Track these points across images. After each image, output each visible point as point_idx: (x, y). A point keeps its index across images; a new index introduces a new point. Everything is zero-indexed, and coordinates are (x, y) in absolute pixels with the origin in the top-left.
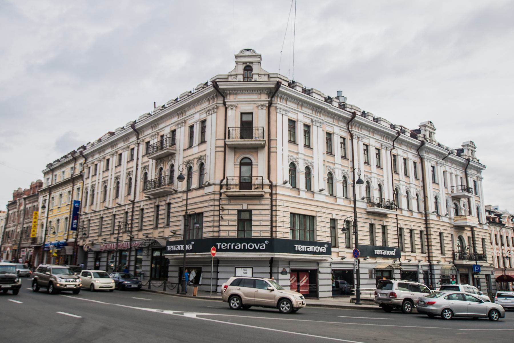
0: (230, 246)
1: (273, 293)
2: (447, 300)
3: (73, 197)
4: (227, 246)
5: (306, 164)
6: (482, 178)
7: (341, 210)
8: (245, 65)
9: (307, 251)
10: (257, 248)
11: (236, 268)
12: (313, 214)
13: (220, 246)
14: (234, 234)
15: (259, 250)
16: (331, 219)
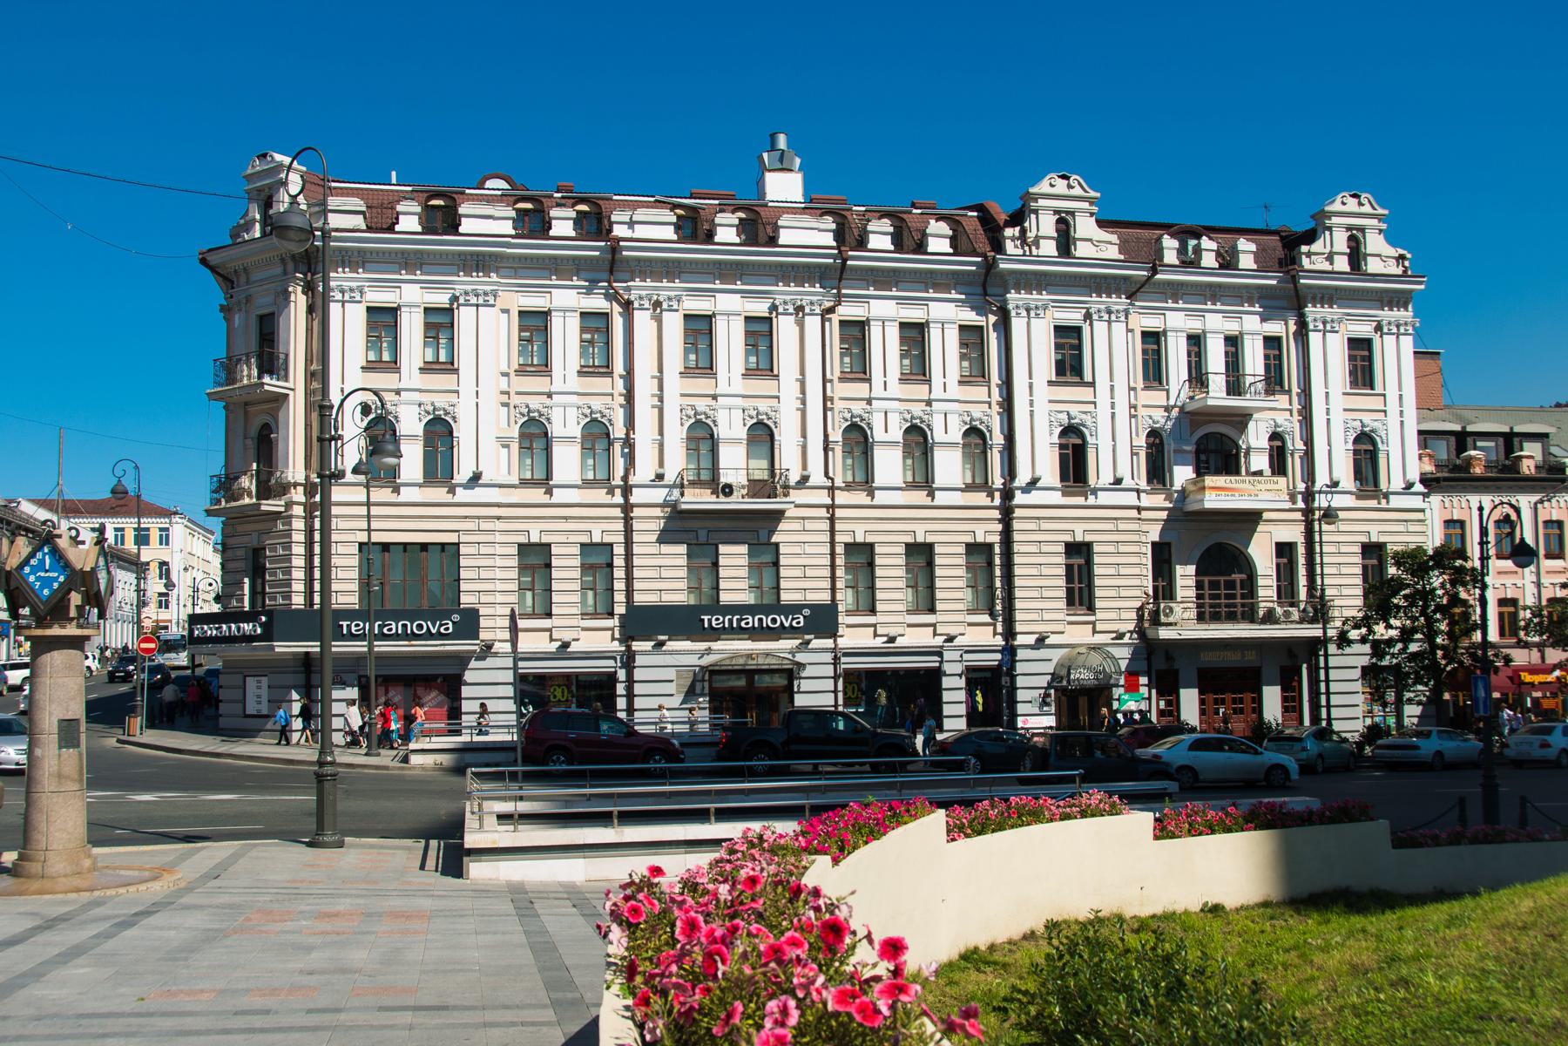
0: (731, 621)
2: (366, 757)
4: (724, 622)
5: (906, 420)
6: (221, 311)
7: (466, 517)
8: (1349, 233)
10: (434, 631)
11: (245, 676)
12: (451, 538)
13: (710, 621)
15: (440, 636)
16: (524, 549)
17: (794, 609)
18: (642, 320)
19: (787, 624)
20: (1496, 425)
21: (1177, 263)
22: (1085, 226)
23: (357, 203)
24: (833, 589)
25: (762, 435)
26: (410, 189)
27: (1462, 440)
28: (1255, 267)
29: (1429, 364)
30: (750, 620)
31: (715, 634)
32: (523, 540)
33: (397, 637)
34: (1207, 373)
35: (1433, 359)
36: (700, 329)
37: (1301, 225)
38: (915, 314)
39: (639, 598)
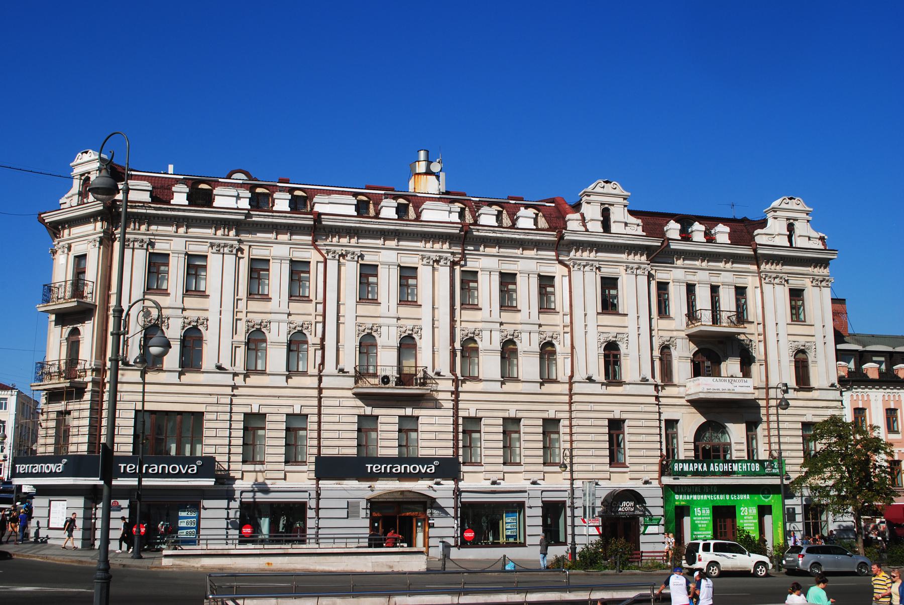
0: (386, 468)
1: (434, 481)
3: (750, 392)
4: (381, 469)
9: (32, 473)
10: (184, 472)
13: (372, 468)
14: (395, 452)
15: (187, 475)
17: (427, 461)
18: (332, 265)
19: (423, 471)
20: (857, 346)
21: (680, 238)
22: (618, 214)
23: (147, 185)
24: (456, 447)
25: (407, 344)
26: (182, 177)
27: (862, 357)
28: (729, 242)
29: (839, 307)
30: (399, 468)
31: (374, 477)
32: (248, 410)
33: (157, 475)
34: (720, 311)
35: (840, 304)
36: (368, 272)
37: (753, 216)
38: (508, 268)
39: (325, 452)
